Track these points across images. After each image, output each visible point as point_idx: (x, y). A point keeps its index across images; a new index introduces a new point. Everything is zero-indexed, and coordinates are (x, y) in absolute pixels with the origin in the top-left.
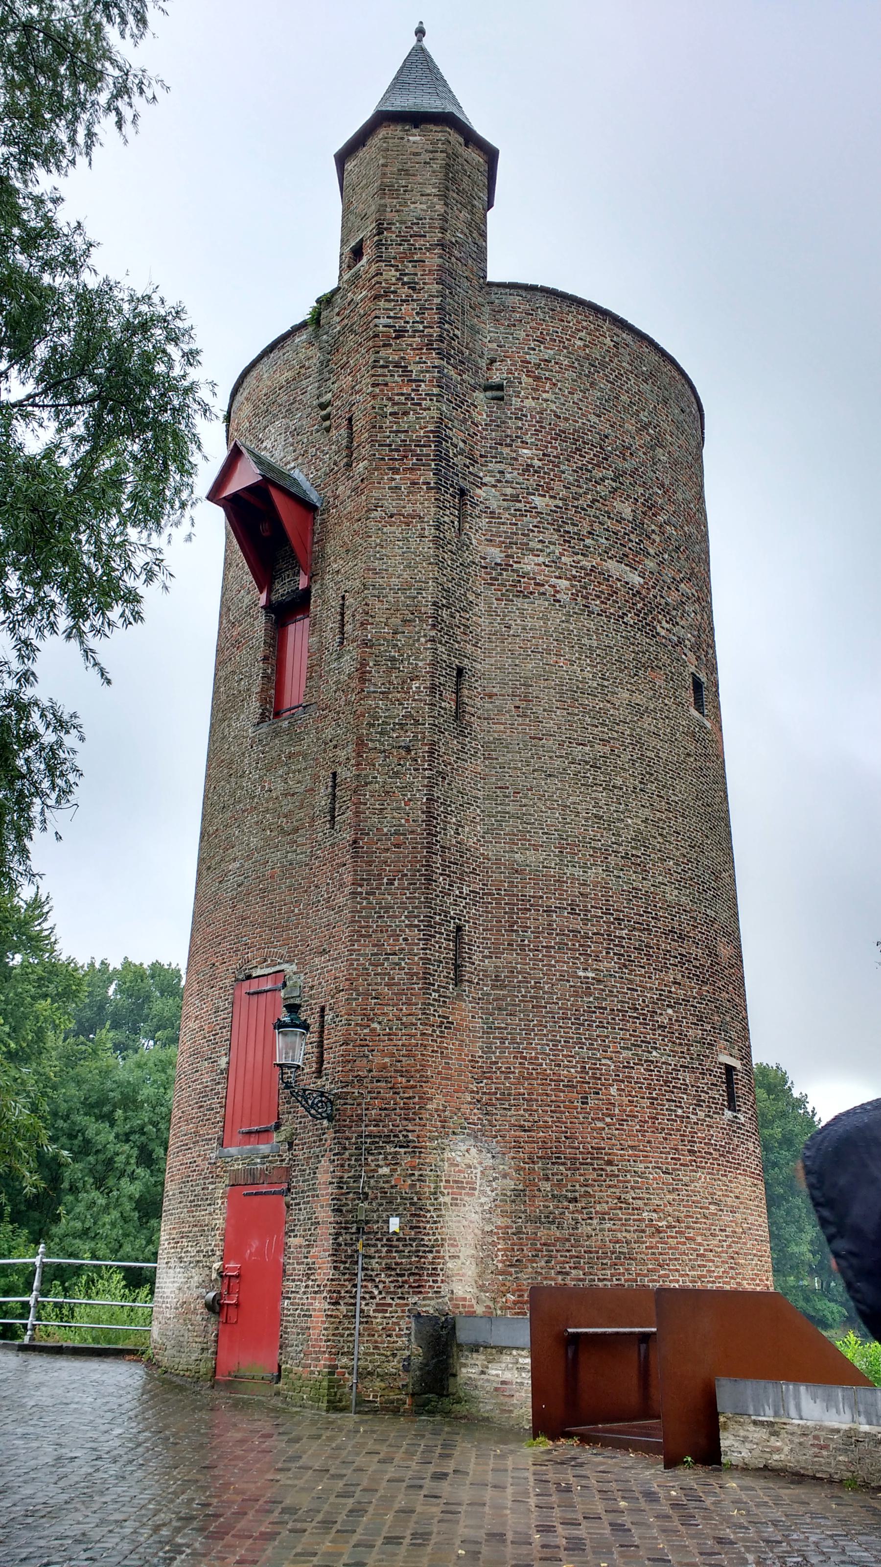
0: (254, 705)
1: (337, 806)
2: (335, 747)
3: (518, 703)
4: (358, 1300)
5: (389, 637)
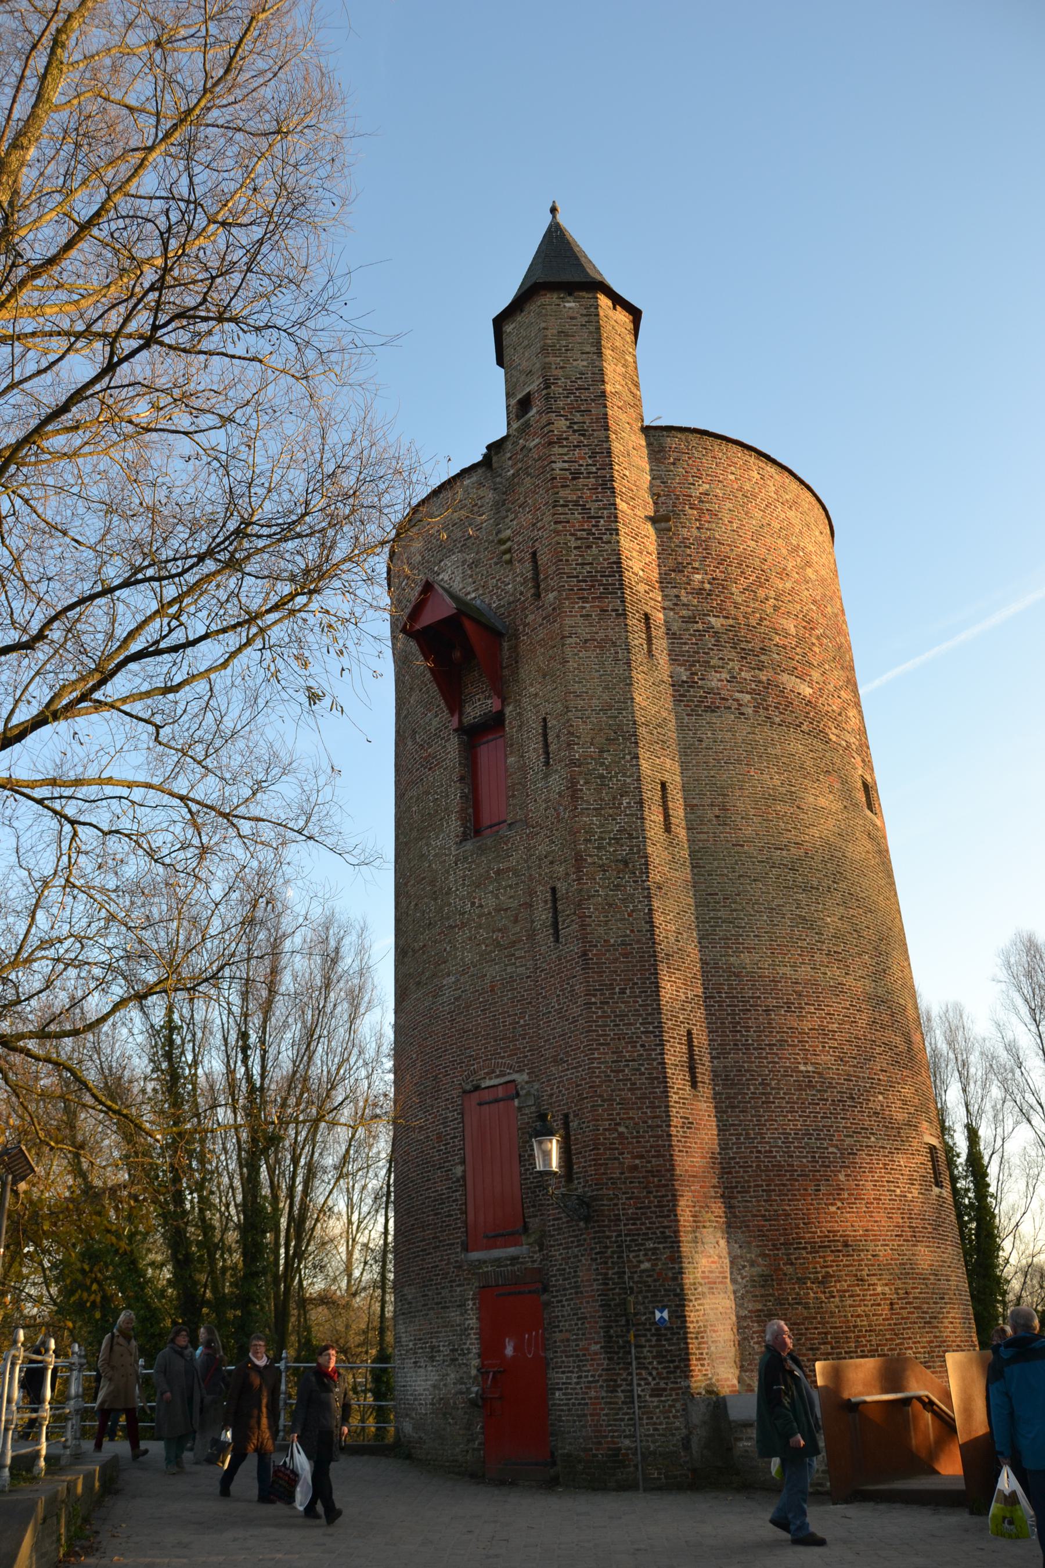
0: (454, 825)
1: (560, 919)
2: (552, 863)
3: (717, 812)
4: (635, 1387)
5: (596, 756)
